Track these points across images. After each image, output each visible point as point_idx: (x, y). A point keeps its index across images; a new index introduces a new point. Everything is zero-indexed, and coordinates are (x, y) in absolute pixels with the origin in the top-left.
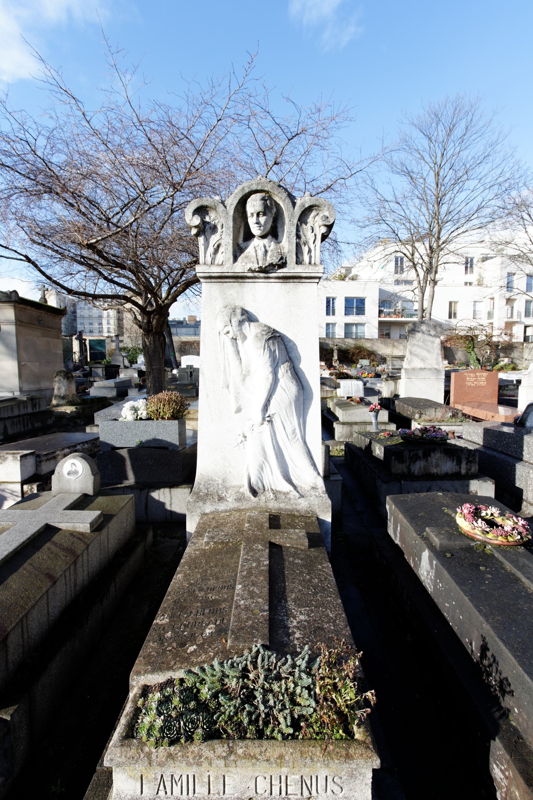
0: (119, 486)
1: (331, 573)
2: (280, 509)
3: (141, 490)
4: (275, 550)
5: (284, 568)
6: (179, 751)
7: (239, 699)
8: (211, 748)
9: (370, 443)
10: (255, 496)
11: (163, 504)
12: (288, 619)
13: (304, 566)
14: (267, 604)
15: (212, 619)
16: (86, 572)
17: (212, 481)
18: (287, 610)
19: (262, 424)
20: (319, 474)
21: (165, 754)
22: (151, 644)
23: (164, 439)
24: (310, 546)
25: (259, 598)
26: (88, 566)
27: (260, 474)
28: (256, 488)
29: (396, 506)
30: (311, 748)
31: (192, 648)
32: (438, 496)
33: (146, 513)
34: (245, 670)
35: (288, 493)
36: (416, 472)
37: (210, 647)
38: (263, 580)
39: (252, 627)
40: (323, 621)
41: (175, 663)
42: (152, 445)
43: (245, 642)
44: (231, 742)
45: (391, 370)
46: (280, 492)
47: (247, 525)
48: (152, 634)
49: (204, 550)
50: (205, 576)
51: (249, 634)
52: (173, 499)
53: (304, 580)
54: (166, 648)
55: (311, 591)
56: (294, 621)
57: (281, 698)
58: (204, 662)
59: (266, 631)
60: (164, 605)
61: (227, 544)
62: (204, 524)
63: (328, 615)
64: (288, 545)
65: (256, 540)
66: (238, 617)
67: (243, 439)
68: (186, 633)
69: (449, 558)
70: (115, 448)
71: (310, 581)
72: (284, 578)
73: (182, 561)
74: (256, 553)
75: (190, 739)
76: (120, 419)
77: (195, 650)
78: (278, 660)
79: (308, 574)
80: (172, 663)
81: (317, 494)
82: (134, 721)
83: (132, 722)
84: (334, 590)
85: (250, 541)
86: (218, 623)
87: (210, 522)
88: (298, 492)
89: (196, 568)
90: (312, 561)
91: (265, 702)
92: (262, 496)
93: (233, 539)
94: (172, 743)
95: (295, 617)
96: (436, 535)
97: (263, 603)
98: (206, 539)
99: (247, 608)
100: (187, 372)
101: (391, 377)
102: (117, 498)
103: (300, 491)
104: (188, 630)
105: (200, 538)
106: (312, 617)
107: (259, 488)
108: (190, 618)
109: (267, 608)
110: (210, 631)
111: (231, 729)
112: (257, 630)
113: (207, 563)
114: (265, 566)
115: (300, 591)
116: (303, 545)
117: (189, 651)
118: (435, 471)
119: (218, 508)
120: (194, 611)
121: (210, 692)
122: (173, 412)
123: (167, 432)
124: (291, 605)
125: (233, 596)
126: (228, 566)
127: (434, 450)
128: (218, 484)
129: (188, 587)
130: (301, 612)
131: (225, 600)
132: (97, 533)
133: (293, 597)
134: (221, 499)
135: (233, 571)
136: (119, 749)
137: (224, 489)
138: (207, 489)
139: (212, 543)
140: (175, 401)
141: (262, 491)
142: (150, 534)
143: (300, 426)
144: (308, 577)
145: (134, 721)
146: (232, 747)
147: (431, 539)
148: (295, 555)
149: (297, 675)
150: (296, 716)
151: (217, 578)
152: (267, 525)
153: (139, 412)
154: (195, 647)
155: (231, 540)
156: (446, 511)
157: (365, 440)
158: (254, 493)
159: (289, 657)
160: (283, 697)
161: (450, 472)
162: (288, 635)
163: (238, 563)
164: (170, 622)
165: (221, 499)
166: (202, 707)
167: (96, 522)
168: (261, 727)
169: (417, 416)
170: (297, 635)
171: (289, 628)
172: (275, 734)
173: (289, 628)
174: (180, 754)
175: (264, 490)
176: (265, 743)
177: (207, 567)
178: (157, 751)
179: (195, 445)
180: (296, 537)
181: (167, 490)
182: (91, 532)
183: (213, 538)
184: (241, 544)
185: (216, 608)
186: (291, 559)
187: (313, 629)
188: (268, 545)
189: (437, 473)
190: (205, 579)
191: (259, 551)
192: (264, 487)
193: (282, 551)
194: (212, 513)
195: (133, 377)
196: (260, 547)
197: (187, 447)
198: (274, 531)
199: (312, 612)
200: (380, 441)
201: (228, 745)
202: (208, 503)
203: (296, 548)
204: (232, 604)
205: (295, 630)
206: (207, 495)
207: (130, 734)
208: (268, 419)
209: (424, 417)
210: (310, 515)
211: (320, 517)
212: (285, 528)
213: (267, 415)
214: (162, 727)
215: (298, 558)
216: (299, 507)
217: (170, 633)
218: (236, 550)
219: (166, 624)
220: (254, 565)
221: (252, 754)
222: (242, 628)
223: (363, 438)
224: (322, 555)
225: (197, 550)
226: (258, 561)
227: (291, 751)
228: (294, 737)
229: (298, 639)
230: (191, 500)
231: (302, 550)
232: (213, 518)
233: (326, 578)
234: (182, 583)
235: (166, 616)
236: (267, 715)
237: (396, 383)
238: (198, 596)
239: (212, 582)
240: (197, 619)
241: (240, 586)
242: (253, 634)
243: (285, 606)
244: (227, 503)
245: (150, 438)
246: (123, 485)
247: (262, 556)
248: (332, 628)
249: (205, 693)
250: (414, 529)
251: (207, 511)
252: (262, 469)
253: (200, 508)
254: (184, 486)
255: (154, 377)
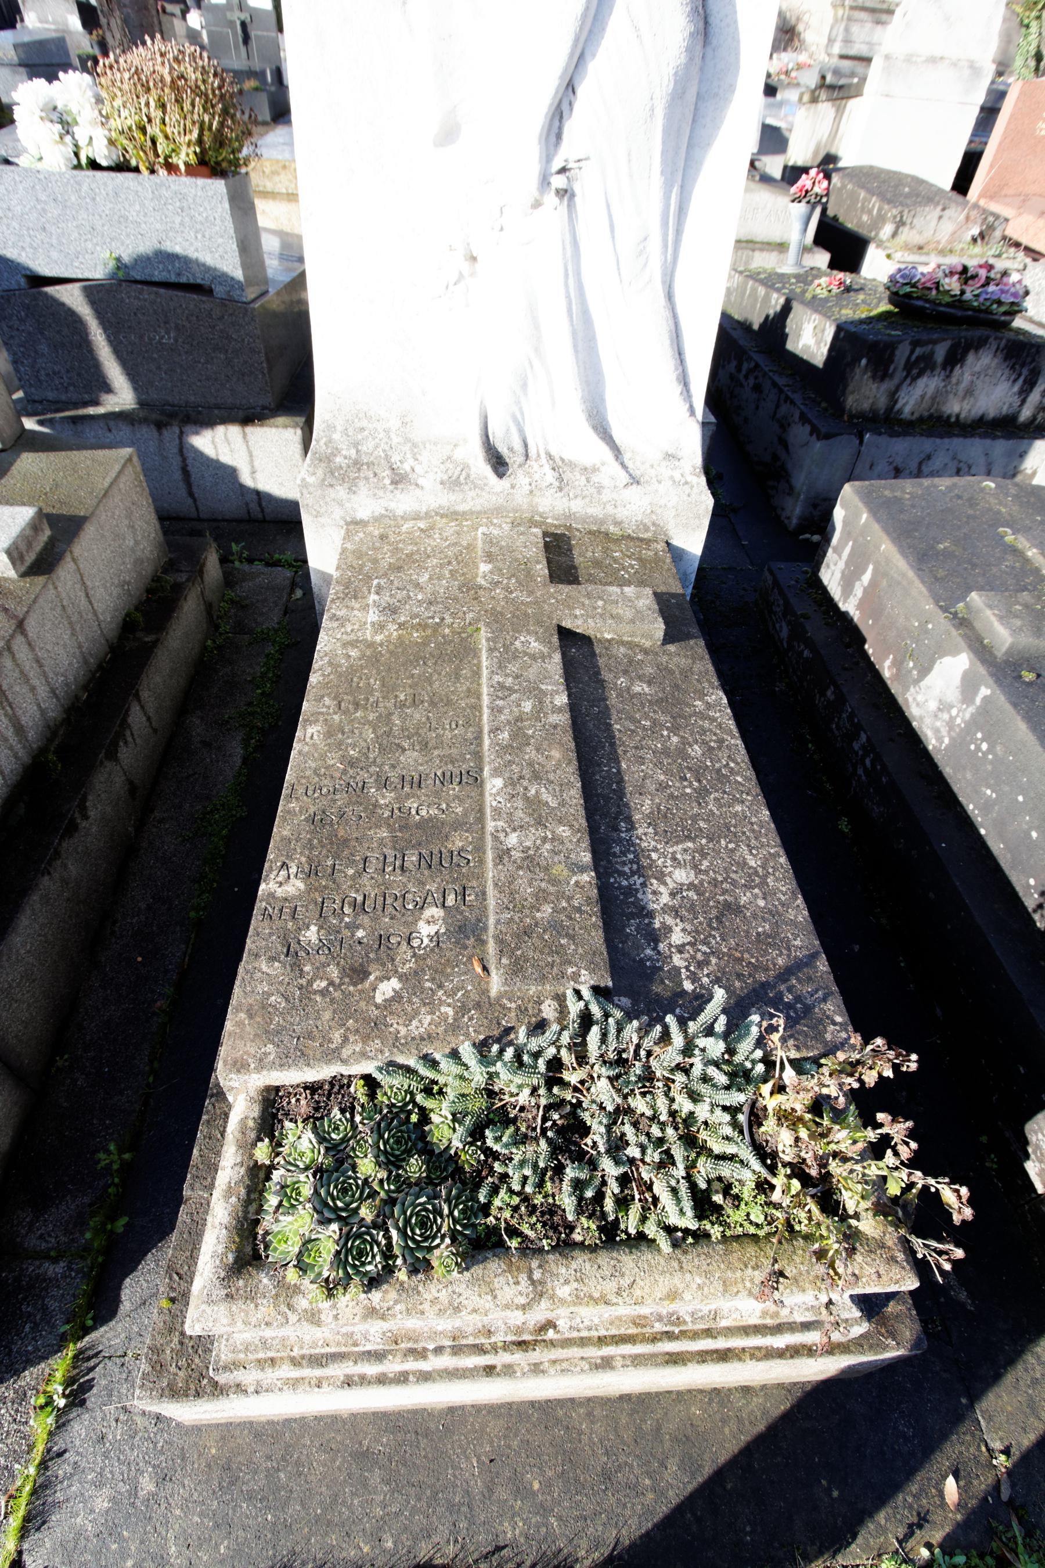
0: (91, 411)
1: (732, 724)
2: (570, 516)
3: (160, 426)
4: (575, 647)
5: (606, 712)
6: (396, 1302)
7: (543, 1143)
8: (485, 1289)
9: (787, 309)
10: (501, 475)
11: (232, 472)
12: (644, 885)
13: (659, 702)
14: (586, 844)
15: (432, 887)
16: (43, 691)
17: (370, 419)
18: (639, 854)
19: (537, 204)
20: (692, 412)
21: (359, 1310)
22: (264, 968)
23: (193, 254)
24: (670, 638)
25: (560, 822)
26: (45, 674)
27: (518, 403)
28: (503, 450)
29: (874, 512)
30: (750, 1270)
31: (387, 988)
32: (982, 490)
33: (191, 494)
34: (556, 1064)
35: (595, 470)
36: (907, 410)
37: (440, 986)
38: (560, 759)
39: (555, 926)
40: (734, 883)
41: (345, 1039)
42: (158, 276)
43: (543, 979)
44: (535, 1264)
45: (835, 61)
46: (572, 465)
47: (484, 568)
48: (260, 935)
49: (371, 645)
50: (388, 734)
51: (551, 953)
52: (256, 456)
53: (666, 752)
54: (310, 983)
55: (691, 785)
56: (662, 889)
57: (655, 1131)
58: (429, 1038)
59: (597, 938)
60: (280, 830)
61: (435, 631)
62: (359, 554)
63: (745, 863)
64: (608, 636)
65: (520, 622)
66: (507, 887)
67: (466, 267)
68: (360, 934)
69: (1030, 684)
70: (39, 281)
71: (682, 752)
72: (613, 745)
73: (314, 679)
74: (525, 667)
75: (420, 1267)
76: (23, 161)
77: (397, 997)
78: (644, 1031)
79: (675, 729)
80: (337, 1036)
81: (677, 476)
82: (253, 1208)
83: (246, 1212)
84: (746, 778)
85: (506, 622)
86: (450, 900)
87: (374, 549)
88: (624, 466)
89: (357, 705)
90: (677, 687)
91: (616, 1147)
92: (520, 473)
93: (454, 615)
94: (373, 1283)
95: (661, 878)
96: (1001, 618)
97: (571, 838)
98: (373, 616)
99: (530, 861)
100: (231, 24)
101: (832, 87)
102: (83, 458)
103: (629, 464)
104: (365, 920)
105: (353, 603)
106: (706, 872)
107: (511, 449)
108: (365, 880)
109: (587, 857)
110: (432, 929)
111: (532, 1227)
112: (572, 937)
113: (388, 689)
114: (560, 710)
115: (662, 787)
116: (649, 636)
117: (379, 999)
118: (956, 409)
119: (392, 505)
120: (374, 856)
121: (460, 1129)
122: (200, 141)
123: (186, 222)
124: (645, 835)
125: (481, 820)
126: (449, 703)
127: (978, 345)
128: (387, 431)
129: (344, 772)
130: (674, 859)
131: (458, 825)
132: (41, 580)
133: (646, 808)
134: (399, 479)
135: (468, 724)
136: (222, 1309)
137: (407, 448)
138: (356, 445)
139: (392, 627)
140: (196, 90)
141: (520, 459)
142: (212, 561)
143: (665, 223)
144: (675, 739)
145: (253, 1208)
146: (542, 1283)
147: (978, 625)
148: (629, 668)
149: (697, 1071)
150: (703, 1186)
151: (425, 746)
152: (541, 569)
153: (81, 133)
154: (394, 983)
155: (448, 620)
156: (1009, 538)
157: (767, 298)
158: (499, 463)
159: (669, 1019)
160: (662, 1130)
161: (992, 413)
162: (654, 938)
163: (479, 697)
164: (310, 889)
165: (399, 479)
166: (443, 1166)
167: (30, 545)
168: (611, 1218)
169: (888, 229)
170: (677, 937)
171: (651, 915)
172: (651, 1229)
173: (651, 915)
174: (398, 1307)
175: (527, 456)
176: (627, 1260)
177: (390, 705)
178: (334, 1306)
179: (299, 282)
180: (629, 614)
181: (234, 431)
182: (23, 575)
183: (393, 610)
184: (478, 629)
185: (436, 851)
186: (622, 681)
187: (714, 913)
188: (555, 639)
189: (958, 416)
190: (389, 746)
191: (533, 657)
192: (526, 446)
193: (593, 654)
194: (377, 519)
195: (67, 31)
196: (535, 646)
197: (272, 291)
198: (566, 589)
199: (704, 856)
200: (816, 304)
201: (530, 1278)
202: (363, 489)
203: (630, 645)
204: (482, 838)
205: (670, 921)
206: (357, 464)
207: (248, 1249)
208: (559, 182)
209: (906, 235)
210: (646, 536)
211: (675, 542)
212: (592, 580)
213: (557, 164)
214: (338, 1253)
215: (640, 678)
216: (622, 514)
217: (314, 928)
218: (463, 650)
219: (300, 897)
220: (527, 706)
221: (596, 1295)
222: (527, 932)
223: (761, 291)
224: (698, 667)
225: (353, 644)
226: (540, 697)
227: (698, 1280)
228: (700, 1236)
229: (681, 949)
230: (311, 480)
231: (646, 652)
232: (383, 537)
233: (721, 741)
234: (323, 757)
235: (293, 870)
236: (624, 1180)
237: (840, 112)
238: (376, 805)
239: (411, 759)
240: (388, 885)
241: (499, 782)
242: (560, 950)
243: (630, 842)
244: (418, 491)
245: (145, 246)
246: (101, 410)
247: (546, 677)
248: (761, 903)
249: (447, 1133)
250: (930, 590)
251: (363, 514)
252: (524, 386)
253: (341, 504)
254: (281, 420)
255: (126, 21)
